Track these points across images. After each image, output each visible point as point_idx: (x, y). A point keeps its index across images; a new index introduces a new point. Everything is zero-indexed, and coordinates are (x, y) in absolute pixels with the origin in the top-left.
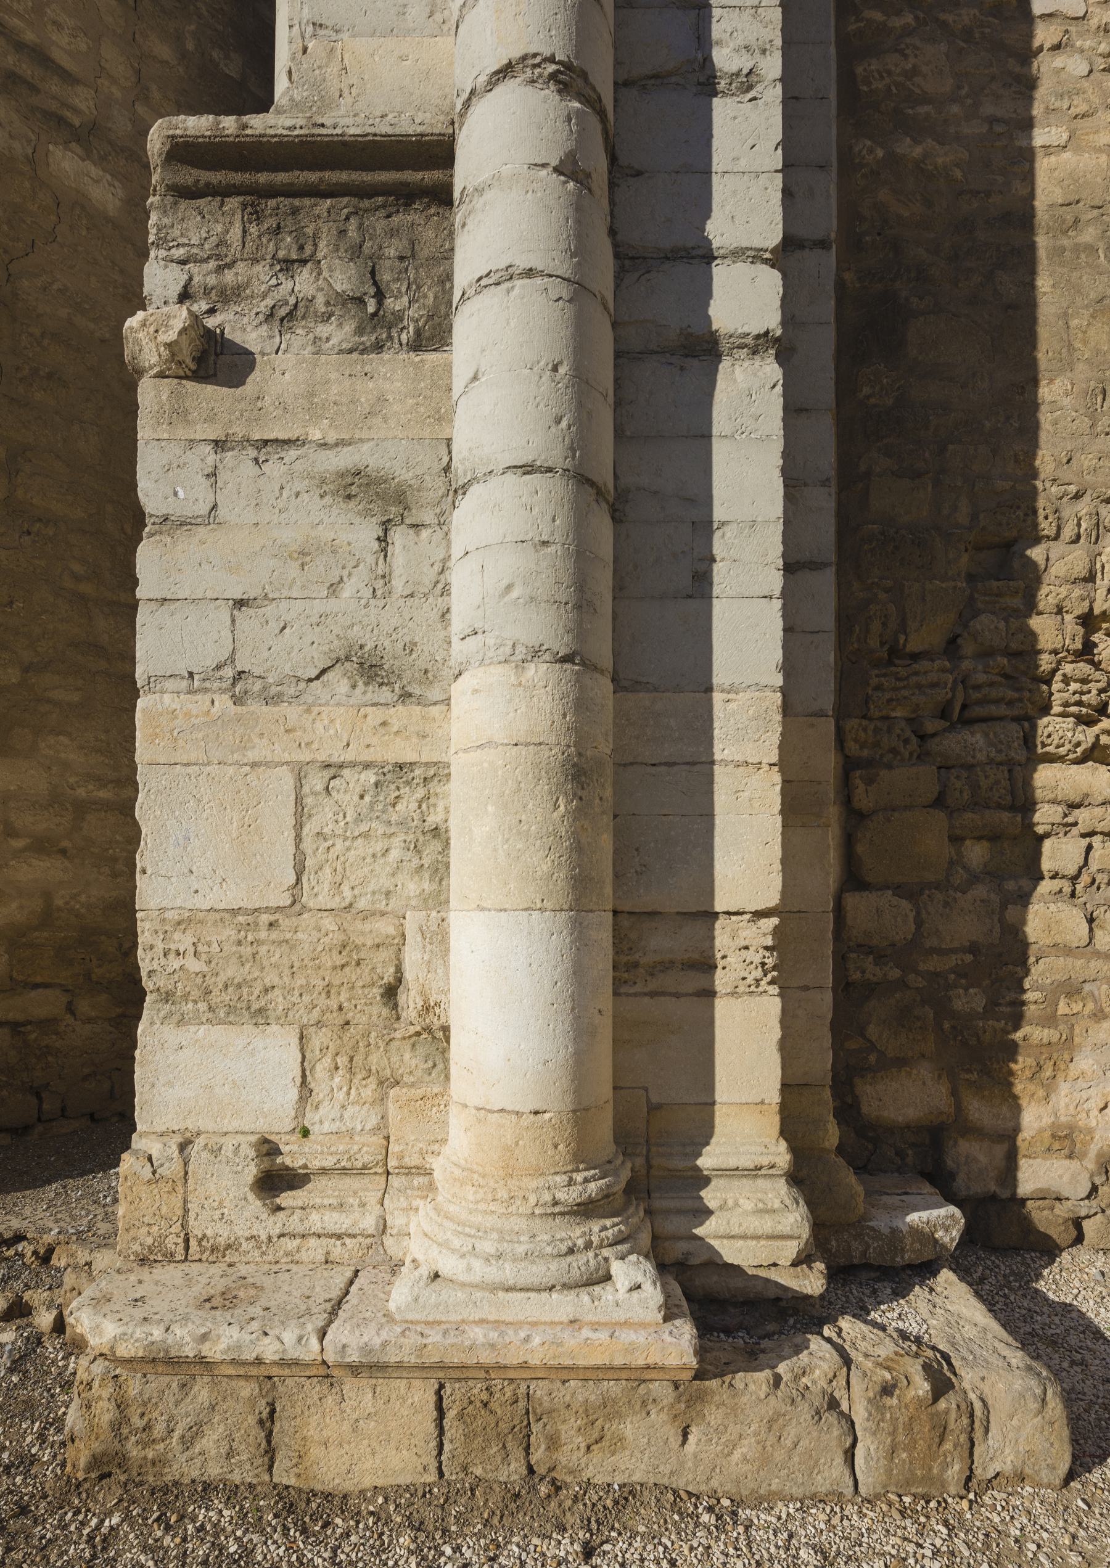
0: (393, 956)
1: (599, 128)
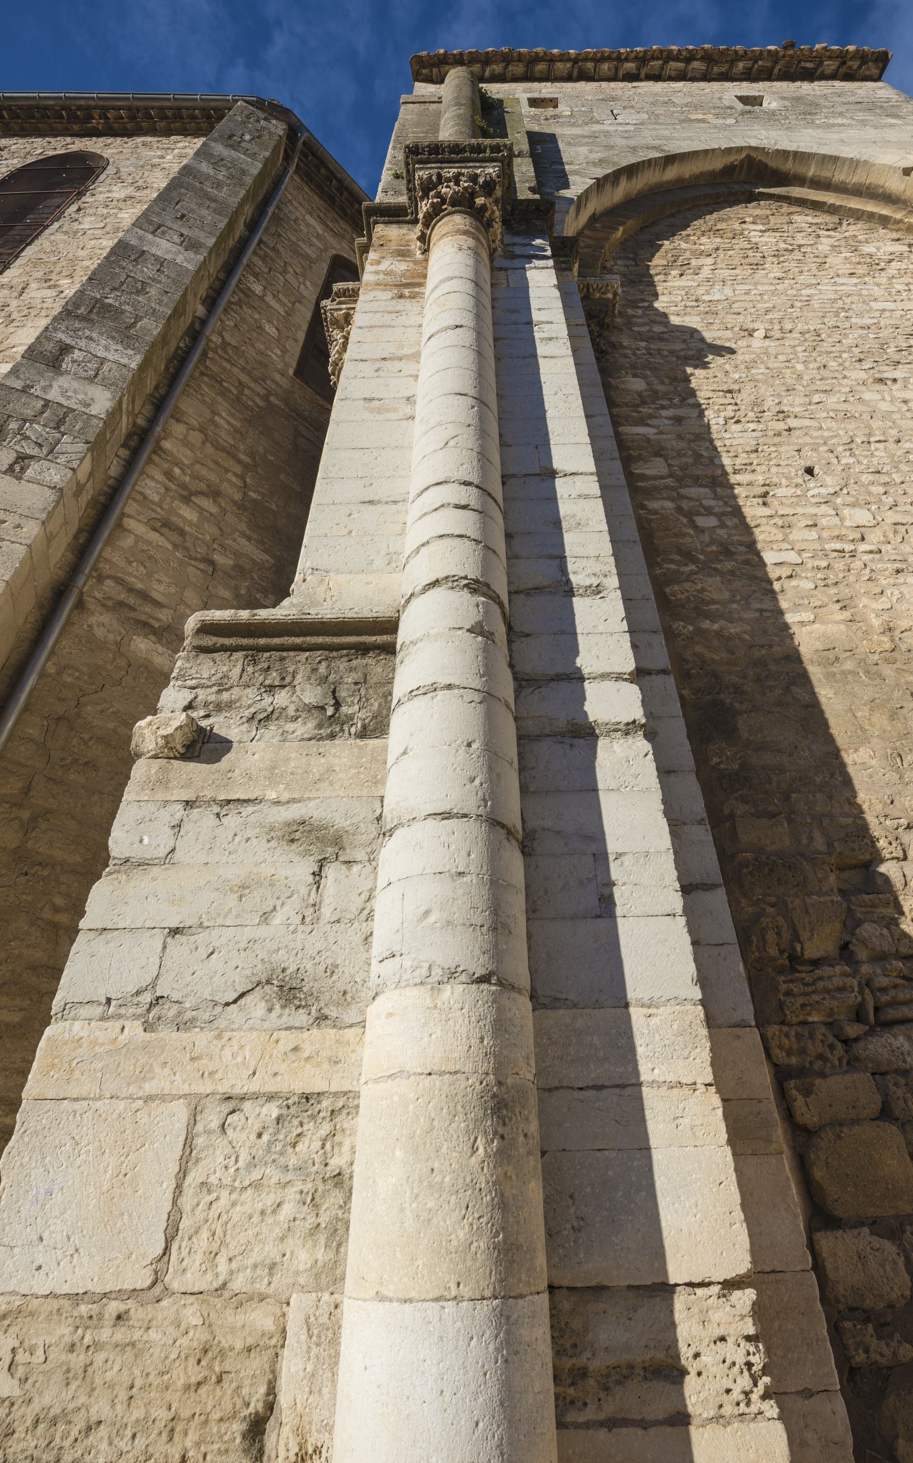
0: (267, 1367)
1: (499, 611)
